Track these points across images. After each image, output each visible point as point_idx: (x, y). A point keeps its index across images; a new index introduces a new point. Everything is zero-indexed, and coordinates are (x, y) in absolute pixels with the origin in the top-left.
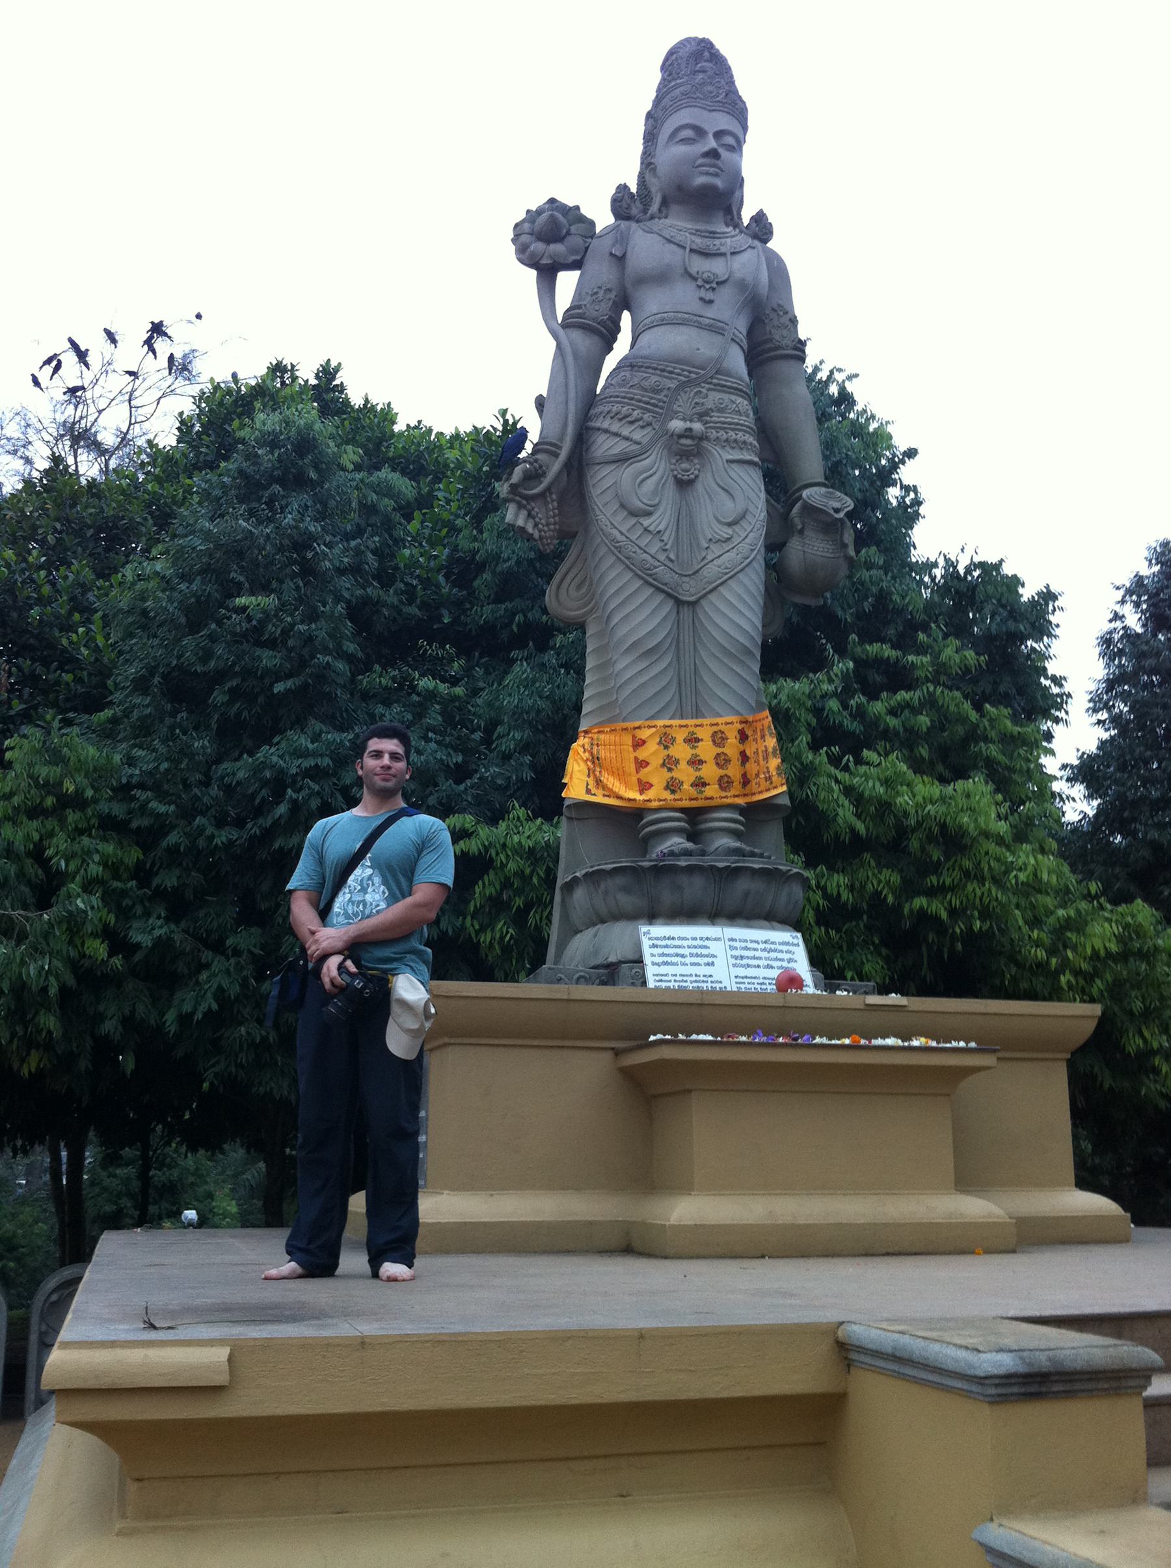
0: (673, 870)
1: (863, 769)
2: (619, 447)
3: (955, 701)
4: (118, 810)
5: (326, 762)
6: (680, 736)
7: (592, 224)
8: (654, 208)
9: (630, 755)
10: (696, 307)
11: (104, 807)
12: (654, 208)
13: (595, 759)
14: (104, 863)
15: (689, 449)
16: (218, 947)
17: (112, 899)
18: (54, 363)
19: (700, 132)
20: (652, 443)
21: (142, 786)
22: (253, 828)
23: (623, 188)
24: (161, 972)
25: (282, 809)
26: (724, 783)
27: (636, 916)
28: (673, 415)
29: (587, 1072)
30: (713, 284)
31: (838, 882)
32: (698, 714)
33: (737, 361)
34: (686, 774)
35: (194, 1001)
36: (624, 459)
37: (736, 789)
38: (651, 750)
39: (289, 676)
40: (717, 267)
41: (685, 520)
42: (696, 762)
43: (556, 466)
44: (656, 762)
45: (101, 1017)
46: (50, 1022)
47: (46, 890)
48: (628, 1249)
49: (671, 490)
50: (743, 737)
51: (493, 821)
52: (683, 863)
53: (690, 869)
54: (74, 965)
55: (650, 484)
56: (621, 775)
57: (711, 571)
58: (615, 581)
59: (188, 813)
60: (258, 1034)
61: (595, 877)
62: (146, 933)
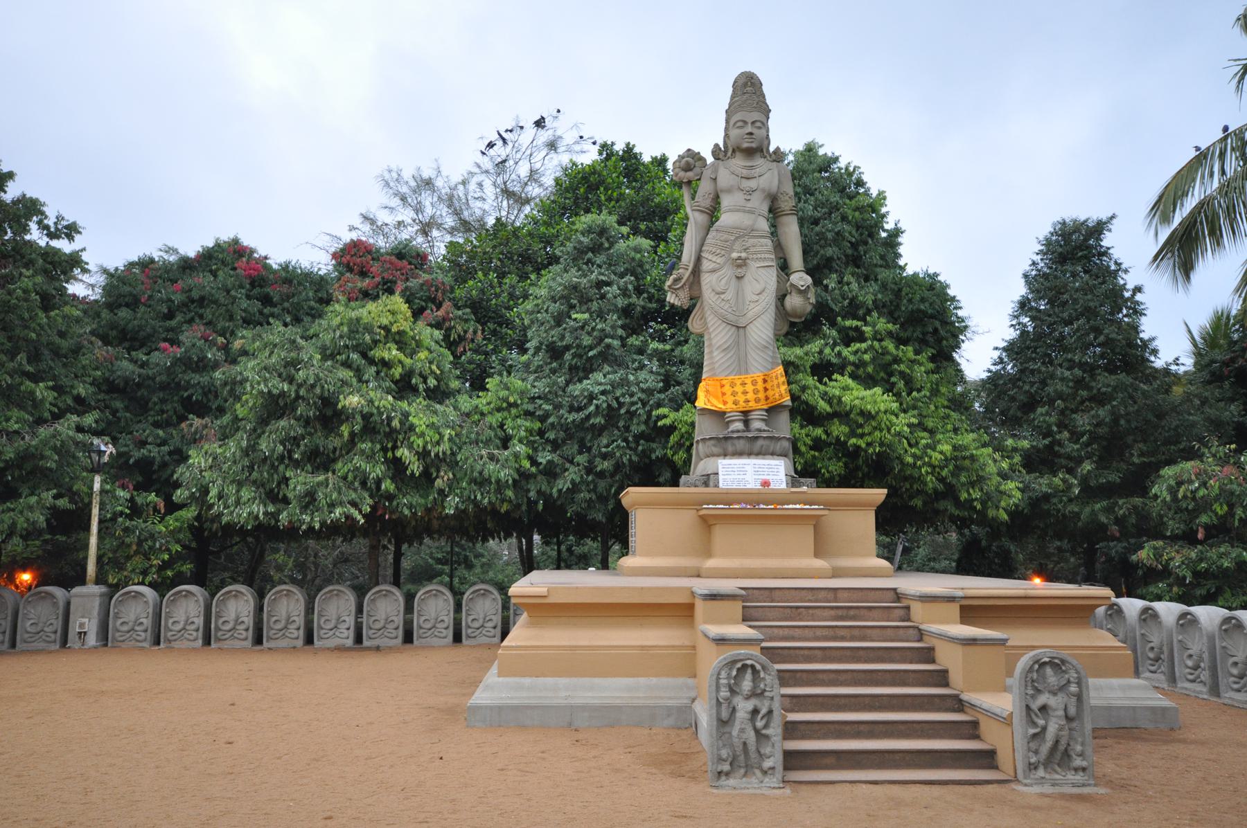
0: (731, 438)
1: (832, 384)
2: (712, 266)
3: (890, 345)
4: (530, 407)
5: (609, 387)
6: (738, 382)
7: (705, 160)
8: (729, 154)
9: (719, 390)
10: (742, 202)
11: (525, 407)
12: (729, 154)
13: (707, 391)
14: (526, 430)
15: (741, 263)
16: (572, 462)
17: (530, 444)
18: (491, 145)
19: (745, 122)
20: (725, 264)
21: (539, 397)
22: (582, 415)
23: (717, 145)
24: (551, 472)
25: (592, 408)
26: (757, 400)
27: (718, 455)
28: (732, 251)
29: (687, 517)
30: (751, 192)
31: (819, 432)
32: (747, 373)
33: (764, 225)
34: (741, 398)
35: (563, 484)
36: (713, 271)
37: (763, 402)
38: (727, 389)
39: (596, 346)
40: (752, 184)
41: (739, 293)
42: (745, 393)
43: (687, 274)
44: (729, 393)
45: (528, 491)
46: (510, 493)
47: (505, 442)
48: (698, 576)
49: (734, 279)
50: (765, 381)
51: (677, 410)
52: (735, 435)
53: (738, 438)
54: (518, 471)
55: (724, 281)
56: (716, 397)
57: (750, 315)
58: (711, 320)
59: (558, 407)
60: (588, 496)
61: (704, 440)
62: (544, 457)
